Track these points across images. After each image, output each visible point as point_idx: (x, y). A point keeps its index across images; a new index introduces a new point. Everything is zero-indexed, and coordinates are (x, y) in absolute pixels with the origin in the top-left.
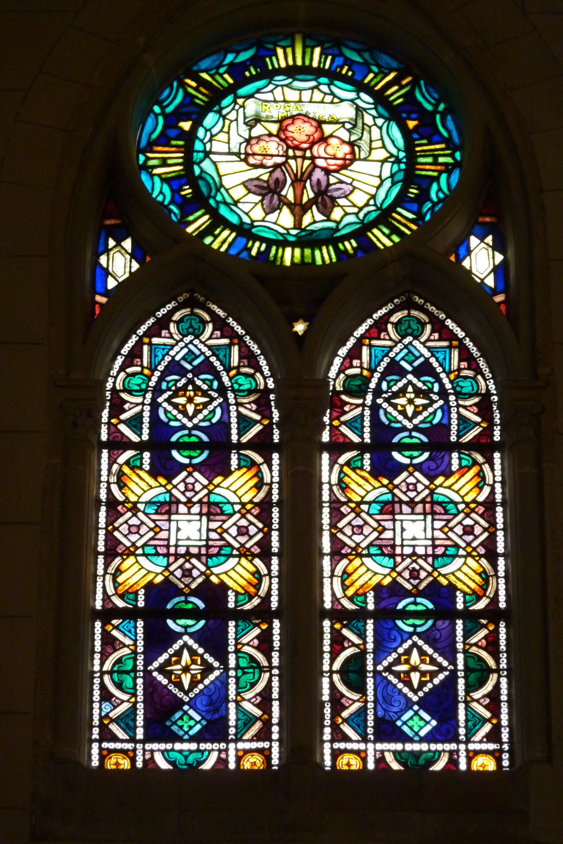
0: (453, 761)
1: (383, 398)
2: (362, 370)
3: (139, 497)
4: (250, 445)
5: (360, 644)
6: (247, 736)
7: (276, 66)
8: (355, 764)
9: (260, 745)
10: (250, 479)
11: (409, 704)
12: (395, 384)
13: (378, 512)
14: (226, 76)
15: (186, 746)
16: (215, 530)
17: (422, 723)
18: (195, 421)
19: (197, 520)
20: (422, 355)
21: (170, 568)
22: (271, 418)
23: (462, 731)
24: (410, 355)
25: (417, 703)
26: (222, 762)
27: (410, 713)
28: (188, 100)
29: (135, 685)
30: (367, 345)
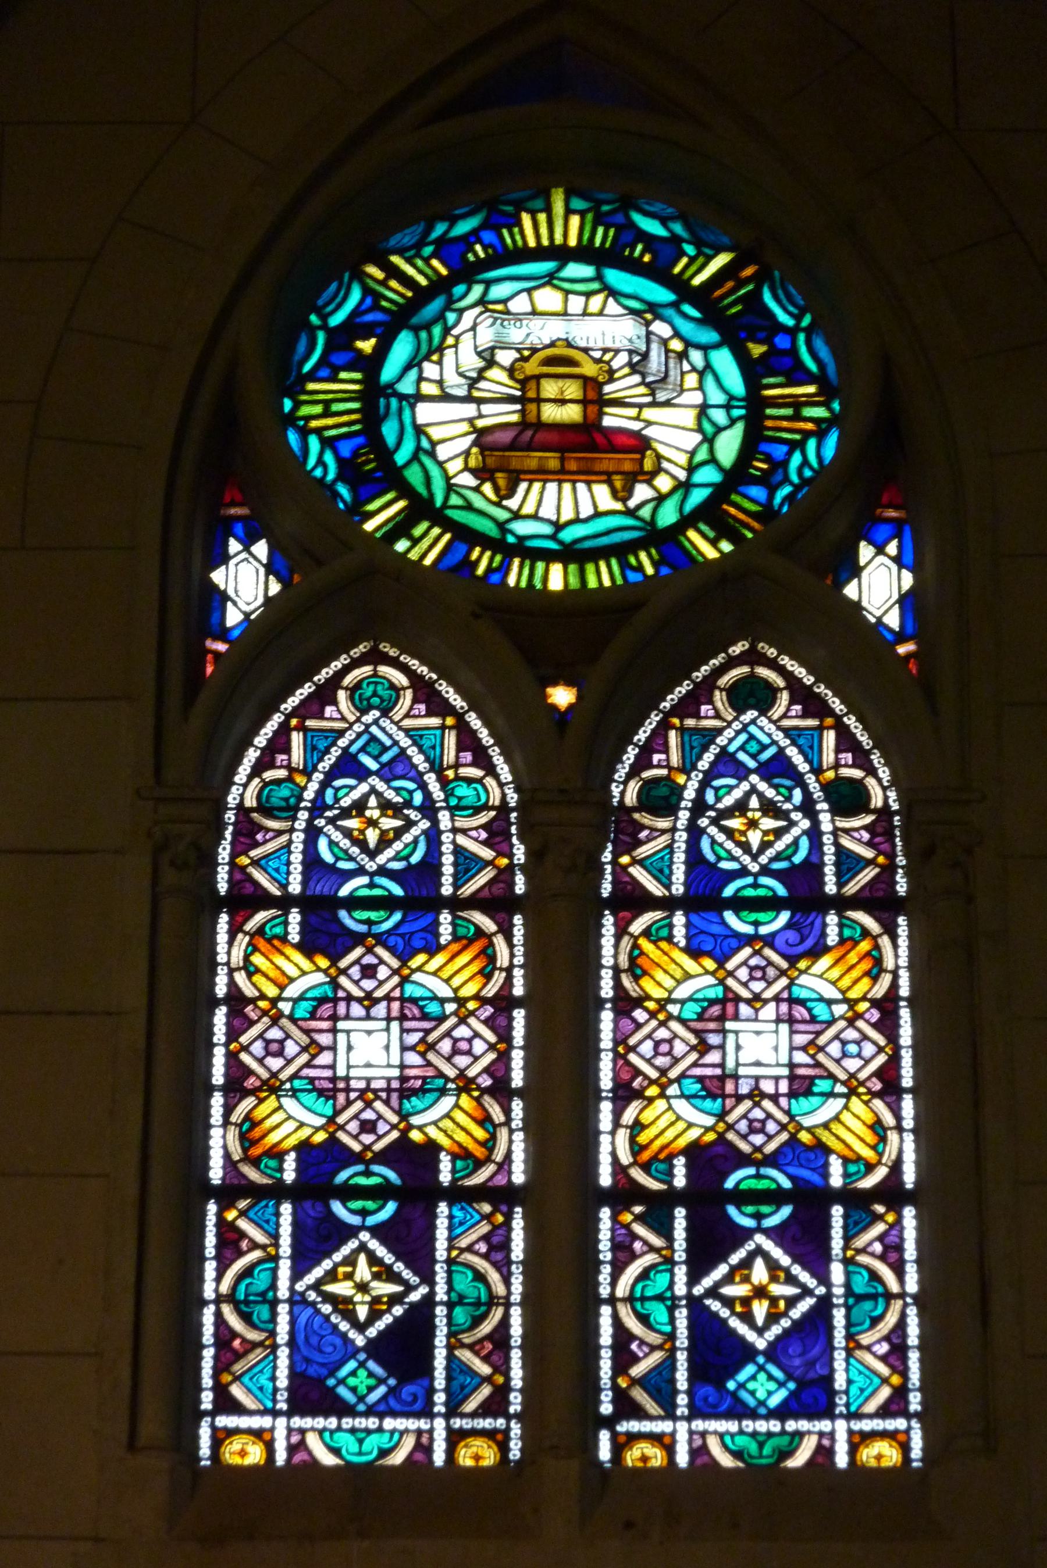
0: (424, 1448)
1: (325, 818)
2: (669, 772)
3: (670, 992)
4: (475, 902)
5: (662, 1249)
6: (470, 1406)
7: (520, 243)
8: (255, 1455)
9: (486, 1423)
10: (288, 958)
11: (350, 1351)
12: (728, 793)
13: (695, 1017)
14: (435, 263)
15: (762, 1426)
16: (413, 1048)
17: (772, 1386)
18: (381, 859)
19: (382, 1030)
20: (774, 743)
21: (727, 1119)
22: (511, 856)
23: (440, 1398)
24: (748, 747)
25: (364, 1349)
26: (824, 1453)
27: (352, 1365)
28: (369, 301)
29: (672, 1320)
30: (677, 729)
